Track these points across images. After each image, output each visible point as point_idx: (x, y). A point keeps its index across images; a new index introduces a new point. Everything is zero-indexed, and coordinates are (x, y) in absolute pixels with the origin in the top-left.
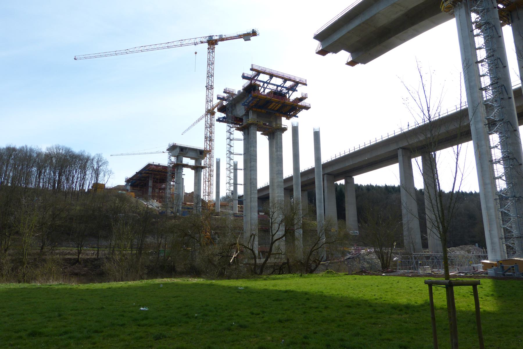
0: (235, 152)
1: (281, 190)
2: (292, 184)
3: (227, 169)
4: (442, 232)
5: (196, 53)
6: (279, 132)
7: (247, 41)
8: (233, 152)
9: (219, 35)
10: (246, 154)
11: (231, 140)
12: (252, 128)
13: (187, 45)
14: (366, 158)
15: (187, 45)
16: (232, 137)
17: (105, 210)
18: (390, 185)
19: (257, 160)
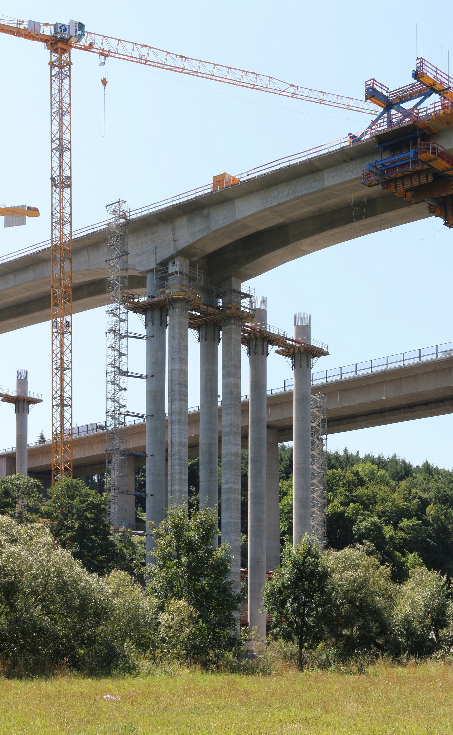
0: (131, 370)
1: (235, 475)
2: (144, 444)
3: (108, 414)
4: (6, 501)
5: (104, 82)
6: (235, 324)
7: (22, 39)
8: (124, 369)
9: (56, 25)
10: (154, 378)
11: (122, 337)
12: (177, 310)
13: (302, 97)
14: (384, 398)
15: (302, 97)
16: (123, 327)
17: (58, 576)
18: (341, 452)
19: (187, 396)
